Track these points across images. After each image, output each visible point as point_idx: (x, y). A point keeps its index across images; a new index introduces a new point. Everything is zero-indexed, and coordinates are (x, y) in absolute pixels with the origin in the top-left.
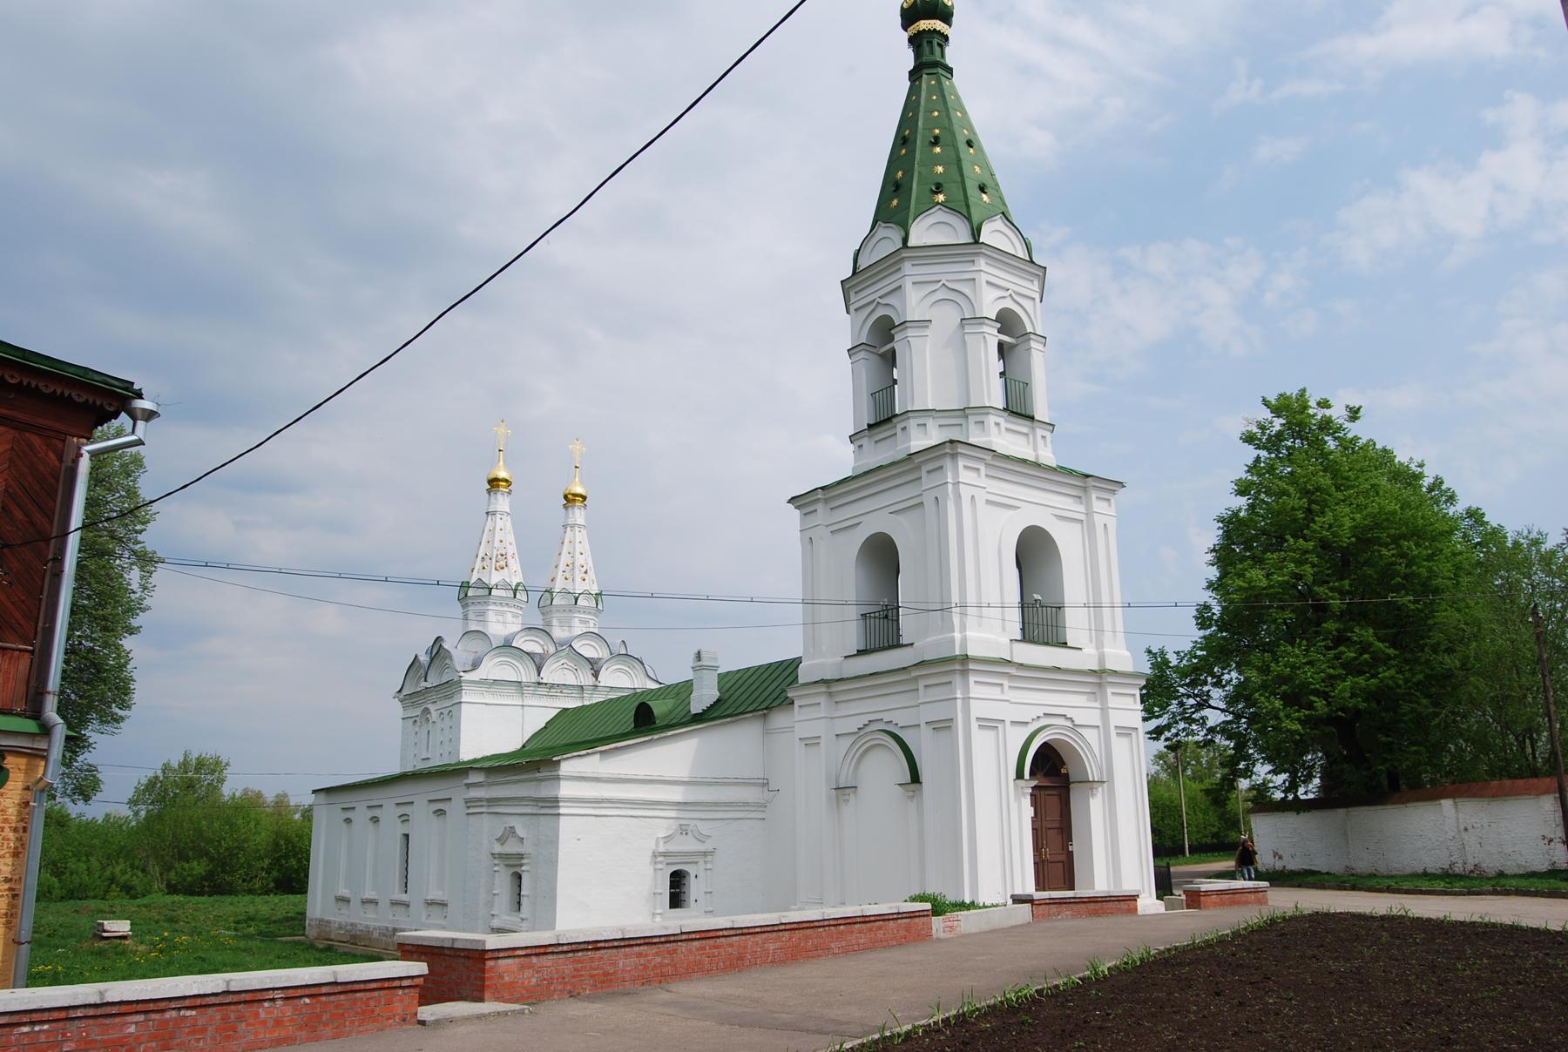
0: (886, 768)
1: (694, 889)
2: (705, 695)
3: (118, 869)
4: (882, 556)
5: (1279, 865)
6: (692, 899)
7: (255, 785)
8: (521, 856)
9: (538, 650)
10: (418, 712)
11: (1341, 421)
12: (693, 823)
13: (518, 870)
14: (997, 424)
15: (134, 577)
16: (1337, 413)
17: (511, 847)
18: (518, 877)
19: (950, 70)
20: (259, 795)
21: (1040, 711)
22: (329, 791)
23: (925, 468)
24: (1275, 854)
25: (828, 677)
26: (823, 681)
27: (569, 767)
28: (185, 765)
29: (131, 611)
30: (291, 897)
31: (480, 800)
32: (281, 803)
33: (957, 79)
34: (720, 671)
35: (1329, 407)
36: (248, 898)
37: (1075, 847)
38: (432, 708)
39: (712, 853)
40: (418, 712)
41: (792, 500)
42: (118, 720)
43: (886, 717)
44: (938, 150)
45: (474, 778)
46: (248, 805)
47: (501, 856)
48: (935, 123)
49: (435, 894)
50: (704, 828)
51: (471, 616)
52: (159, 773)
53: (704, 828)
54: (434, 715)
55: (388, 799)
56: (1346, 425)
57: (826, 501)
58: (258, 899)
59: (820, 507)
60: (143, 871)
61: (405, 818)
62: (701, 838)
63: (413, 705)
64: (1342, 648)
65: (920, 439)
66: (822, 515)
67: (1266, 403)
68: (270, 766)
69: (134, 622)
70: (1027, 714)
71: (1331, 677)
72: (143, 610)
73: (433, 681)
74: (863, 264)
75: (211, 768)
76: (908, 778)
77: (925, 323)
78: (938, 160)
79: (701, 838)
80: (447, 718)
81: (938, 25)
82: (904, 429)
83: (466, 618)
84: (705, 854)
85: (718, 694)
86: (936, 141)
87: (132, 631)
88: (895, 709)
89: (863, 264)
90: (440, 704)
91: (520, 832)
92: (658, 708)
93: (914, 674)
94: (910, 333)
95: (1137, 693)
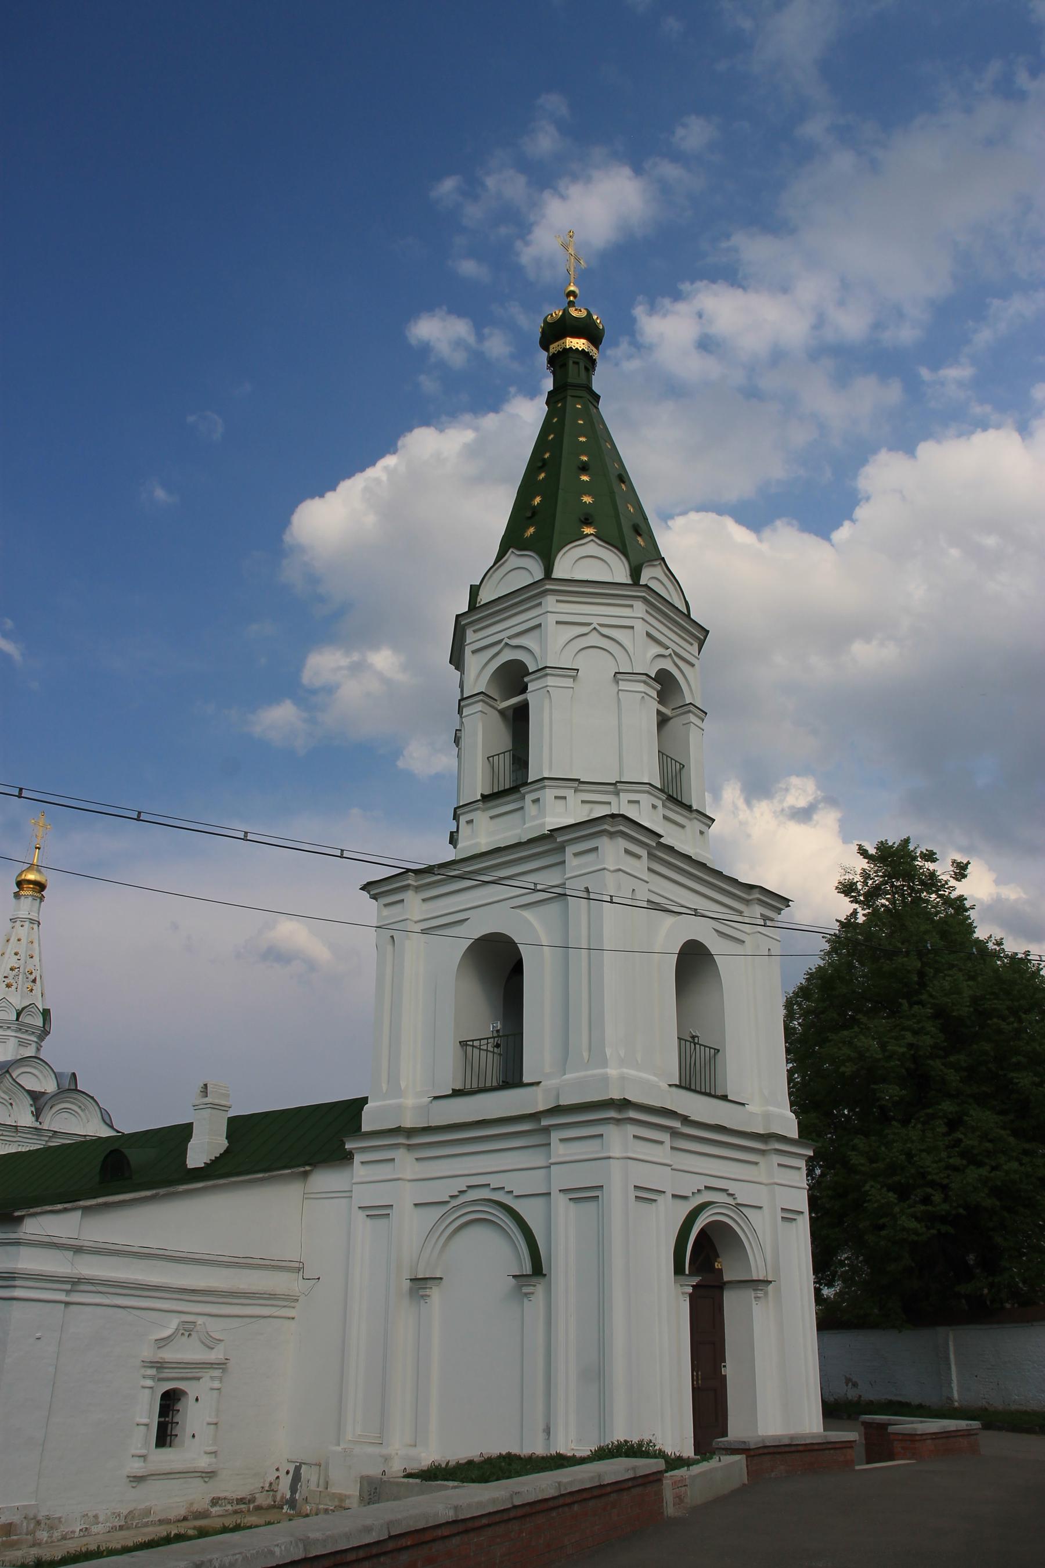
0: (493, 1254)
1: (193, 1417)
4: (499, 966)
5: (852, 1394)
6: (189, 1432)
11: (944, 877)
12: (200, 1320)
14: (654, 807)
16: (942, 869)
19: (597, 398)
21: (701, 1183)
23: (570, 850)
24: (848, 1381)
25: (408, 1123)
26: (397, 1131)
27: (35, 1226)
33: (601, 405)
34: (232, 1113)
35: (934, 861)
37: (730, 1370)
39: (221, 1366)
41: (366, 887)
43: (495, 1181)
44: (585, 478)
48: (583, 448)
50: (216, 1328)
53: (216, 1328)
56: (952, 883)
57: (418, 889)
59: (409, 896)
64: (959, 1135)
65: (557, 812)
66: (415, 907)
67: (863, 852)
70: (688, 1185)
71: (948, 1167)
74: (484, 597)
76: (528, 1269)
77: (573, 673)
78: (586, 488)
81: (579, 344)
82: (536, 801)
86: (584, 468)
88: (510, 1169)
89: (484, 597)
92: (135, 1156)
93: (545, 1122)
94: (550, 681)
95: (802, 1164)
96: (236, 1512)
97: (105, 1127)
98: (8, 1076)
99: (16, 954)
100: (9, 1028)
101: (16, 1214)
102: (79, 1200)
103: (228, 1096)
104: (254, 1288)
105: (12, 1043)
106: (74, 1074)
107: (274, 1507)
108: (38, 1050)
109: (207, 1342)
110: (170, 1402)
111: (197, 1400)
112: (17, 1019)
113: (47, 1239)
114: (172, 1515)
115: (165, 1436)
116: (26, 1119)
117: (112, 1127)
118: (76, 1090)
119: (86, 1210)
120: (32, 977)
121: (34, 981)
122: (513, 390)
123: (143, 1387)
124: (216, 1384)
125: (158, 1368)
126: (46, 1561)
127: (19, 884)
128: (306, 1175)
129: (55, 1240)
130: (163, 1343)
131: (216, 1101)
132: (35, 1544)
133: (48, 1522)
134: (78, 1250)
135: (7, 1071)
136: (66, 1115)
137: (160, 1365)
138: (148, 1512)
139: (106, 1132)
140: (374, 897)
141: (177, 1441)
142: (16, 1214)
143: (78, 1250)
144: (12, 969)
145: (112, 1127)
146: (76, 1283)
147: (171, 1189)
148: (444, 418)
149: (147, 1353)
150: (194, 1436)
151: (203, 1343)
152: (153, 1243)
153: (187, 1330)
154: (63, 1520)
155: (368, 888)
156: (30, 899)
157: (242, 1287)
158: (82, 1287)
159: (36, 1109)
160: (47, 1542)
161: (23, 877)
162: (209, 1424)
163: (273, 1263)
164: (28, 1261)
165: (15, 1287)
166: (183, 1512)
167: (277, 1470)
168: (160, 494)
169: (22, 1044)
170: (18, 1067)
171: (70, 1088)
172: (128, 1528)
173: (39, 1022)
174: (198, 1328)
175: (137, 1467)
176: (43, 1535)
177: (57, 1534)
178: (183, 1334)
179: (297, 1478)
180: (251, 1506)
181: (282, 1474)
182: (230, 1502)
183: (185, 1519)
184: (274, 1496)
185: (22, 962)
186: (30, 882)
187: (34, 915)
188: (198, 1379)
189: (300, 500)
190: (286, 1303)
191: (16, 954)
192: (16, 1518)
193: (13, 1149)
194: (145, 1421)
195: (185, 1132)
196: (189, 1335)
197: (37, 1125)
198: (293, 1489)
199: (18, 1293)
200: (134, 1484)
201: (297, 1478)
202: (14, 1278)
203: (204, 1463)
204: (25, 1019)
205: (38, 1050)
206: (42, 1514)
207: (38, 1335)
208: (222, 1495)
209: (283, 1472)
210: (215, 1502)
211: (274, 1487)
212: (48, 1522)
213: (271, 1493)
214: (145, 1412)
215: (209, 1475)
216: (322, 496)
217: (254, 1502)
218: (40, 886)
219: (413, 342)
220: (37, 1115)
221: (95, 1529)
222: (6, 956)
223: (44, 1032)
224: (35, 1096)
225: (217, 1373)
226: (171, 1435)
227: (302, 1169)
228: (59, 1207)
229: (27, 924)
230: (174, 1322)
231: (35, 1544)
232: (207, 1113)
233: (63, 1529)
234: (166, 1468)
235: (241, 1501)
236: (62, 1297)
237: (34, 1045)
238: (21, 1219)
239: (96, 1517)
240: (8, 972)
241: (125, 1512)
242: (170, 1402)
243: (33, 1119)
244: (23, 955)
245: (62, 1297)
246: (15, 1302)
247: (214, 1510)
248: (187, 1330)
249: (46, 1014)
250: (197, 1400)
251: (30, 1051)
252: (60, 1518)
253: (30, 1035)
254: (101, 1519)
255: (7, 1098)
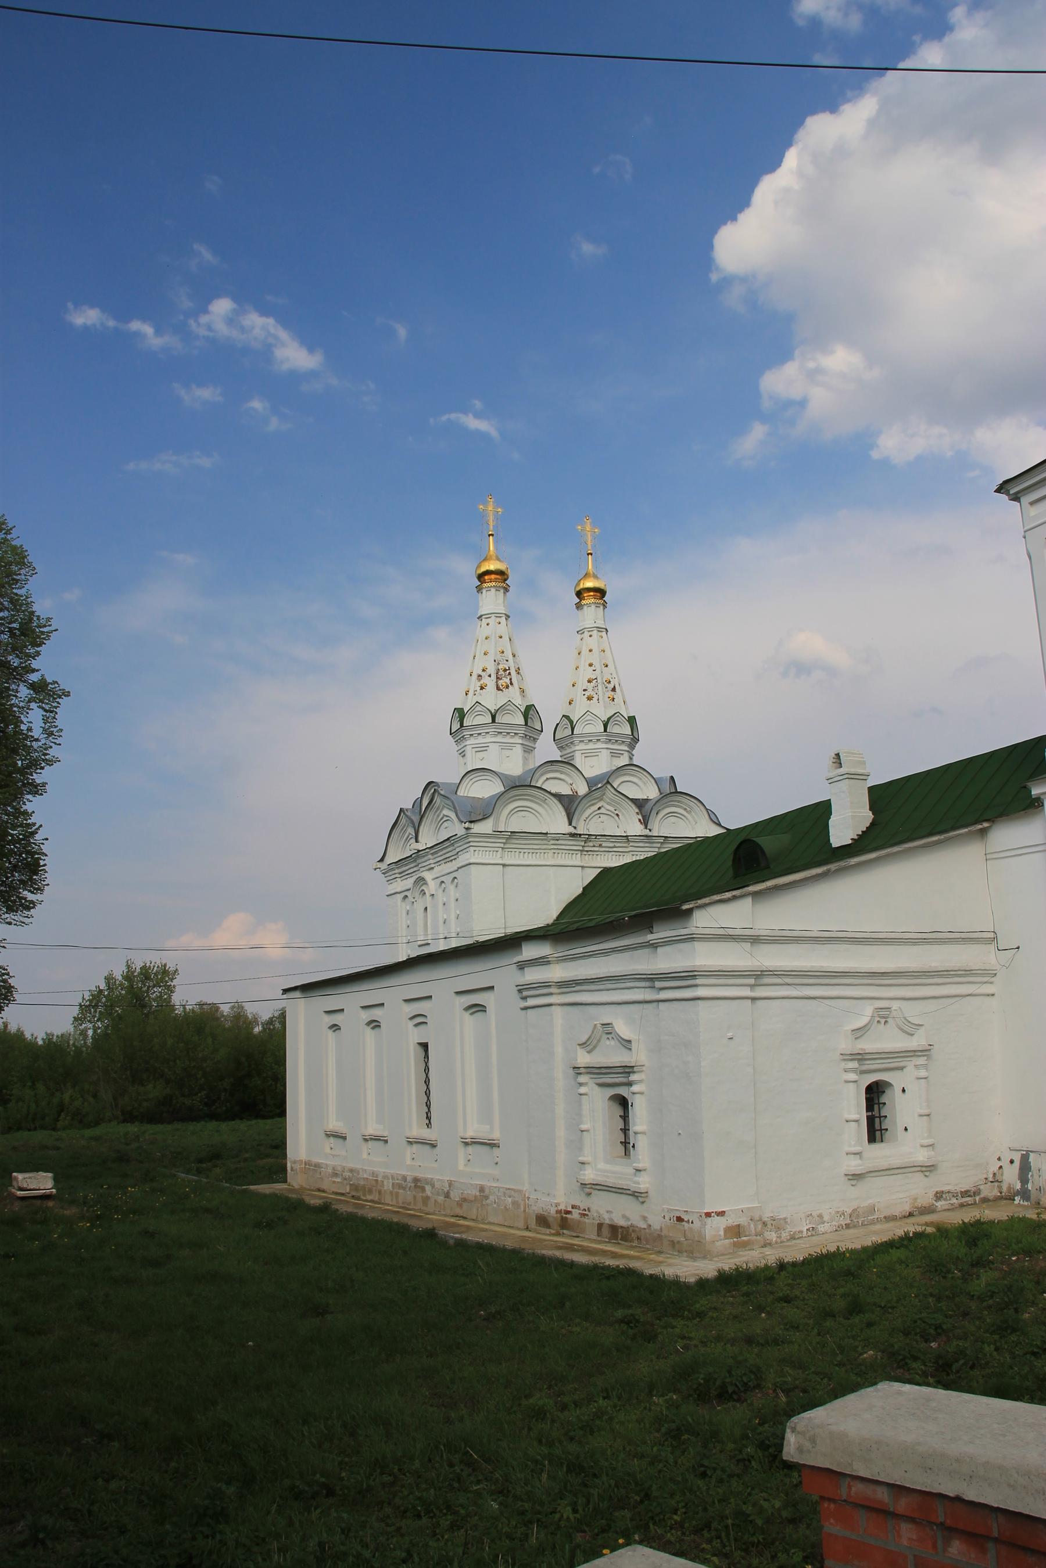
2: (846, 825)
3: (66, 1097)
7: (210, 996)
8: (628, 1070)
9: (566, 791)
10: (409, 882)
12: (895, 1005)
13: (623, 1091)
15: (33, 719)
17: (610, 1055)
18: (623, 1103)
20: (215, 1007)
22: (307, 988)
28: (129, 977)
29: (35, 764)
30: (261, 1122)
31: (546, 985)
32: (240, 1018)
34: (872, 782)
36: (212, 1125)
38: (428, 876)
39: (925, 1052)
40: (409, 882)
41: (998, 491)
42: (29, 906)
45: (530, 951)
46: (204, 1020)
47: (594, 1071)
49: (474, 1129)
50: (913, 1012)
51: (469, 751)
52: (103, 986)
53: (913, 1012)
54: (432, 886)
55: (391, 993)
58: (224, 1126)
60: (95, 1096)
61: (419, 1020)
62: (909, 1029)
63: (404, 875)
68: (227, 962)
69: (38, 778)
72: (50, 763)
73: (428, 838)
75: (164, 976)
79: (909, 1029)
80: (451, 888)
83: (463, 754)
84: (914, 1053)
85: (869, 816)
87: (36, 789)
90: (438, 870)
91: (623, 1029)
92: (768, 843)
96: (962, 1205)
97: (714, 826)
98: (609, 786)
99: (591, 665)
100: (598, 740)
101: (685, 907)
102: (748, 886)
103: (864, 763)
104: (948, 965)
105: (605, 754)
106: (672, 778)
107: (1001, 1198)
108: (631, 759)
109: (906, 1028)
110: (875, 1093)
111: (904, 1091)
112: (605, 731)
113: (721, 932)
114: (897, 1211)
115: (875, 1131)
116: (635, 828)
117: (719, 825)
118: (676, 792)
119: (755, 895)
120: (611, 686)
121: (614, 689)
122: (916, 38)
123: (847, 1082)
124: (923, 1073)
125: (859, 1060)
126: (788, 1263)
127: (579, 594)
128: (983, 832)
129: (731, 932)
130: (859, 1032)
131: (853, 771)
132: (767, 1244)
133: (774, 1223)
134: (755, 940)
135: (608, 782)
136: (672, 819)
137: (860, 1057)
138: (872, 1209)
139: (714, 831)
140: (1016, 498)
141: (887, 1135)
142: (685, 907)
143: (755, 940)
144: (589, 681)
145: (719, 825)
146: (759, 976)
147: (842, 864)
148: (849, 94)
149: (846, 1045)
150: (906, 1129)
151: (901, 1029)
152: (833, 925)
153: (883, 1016)
154: (788, 1220)
155: (1007, 487)
156: (593, 606)
157: (933, 965)
158: (766, 980)
159: (643, 817)
160: (776, 1242)
161: (581, 586)
162: (921, 1116)
163: (963, 935)
164: (704, 957)
165: (696, 986)
166: (907, 1208)
167: (999, 1159)
168: (587, 248)
169: (615, 754)
170: (617, 777)
171: (671, 792)
172: (855, 1226)
173: (627, 730)
174: (894, 1013)
175: (854, 1165)
176: (772, 1236)
177: (785, 1235)
178: (878, 1022)
179: (1025, 1167)
180: (977, 1198)
181: (1005, 1162)
182: (955, 1195)
183: (911, 1215)
184: (1000, 1187)
185: (598, 671)
186: (589, 590)
187: (600, 623)
188: (902, 1068)
189: (714, 232)
190: (986, 979)
191: (591, 665)
192: (743, 1220)
193: (628, 859)
194: (855, 1117)
195: (822, 811)
196: (886, 1022)
197: (647, 832)
198: (1024, 1180)
199: (701, 992)
200: (853, 1182)
201: (1025, 1167)
202: (694, 977)
203: (922, 1156)
204: (613, 729)
205: (631, 759)
206: (766, 1216)
207: (730, 1035)
208: (945, 1188)
209: (1005, 1162)
210: (939, 1196)
211: (998, 1177)
212: (774, 1223)
213: (996, 1184)
214: (855, 1108)
215: (928, 1169)
216: (734, 219)
217: (979, 1194)
218: (601, 593)
219: (801, 23)
220: (645, 822)
221: (821, 1228)
222: (581, 668)
223: (635, 740)
224: (640, 804)
225: (921, 1061)
226: (881, 1130)
227: (980, 827)
228: (728, 895)
229: (595, 633)
230: (868, 1010)
231: (767, 1244)
232: (844, 785)
233: (790, 1229)
234: (884, 1164)
235: (965, 1194)
236: (746, 992)
237: (626, 754)
238: (690, 911)
239: (820, 1216)
240: (586, 685)
241: (849, 1211)
242: (875, 1093)
243: (642, 827)
244: (597, 666)
245: (746, 992)
246: (699, 1002)
247: (940, 1204)
248: (883, 1016)
249: (632, 721)
250: (904, 1091)
251: (624, 760)
252: (785, 1219)
253: (620, 744)
254: (826, 1218)
255: (612, 809)
